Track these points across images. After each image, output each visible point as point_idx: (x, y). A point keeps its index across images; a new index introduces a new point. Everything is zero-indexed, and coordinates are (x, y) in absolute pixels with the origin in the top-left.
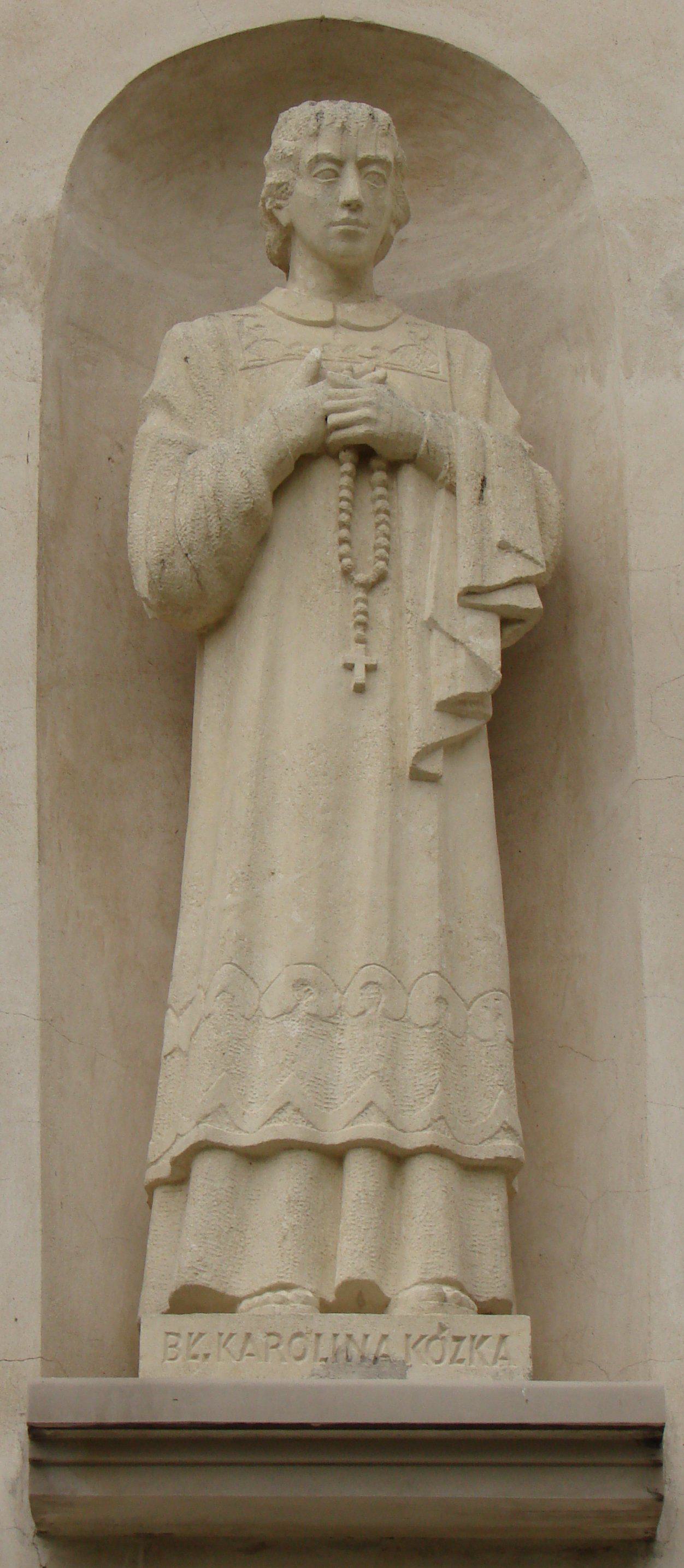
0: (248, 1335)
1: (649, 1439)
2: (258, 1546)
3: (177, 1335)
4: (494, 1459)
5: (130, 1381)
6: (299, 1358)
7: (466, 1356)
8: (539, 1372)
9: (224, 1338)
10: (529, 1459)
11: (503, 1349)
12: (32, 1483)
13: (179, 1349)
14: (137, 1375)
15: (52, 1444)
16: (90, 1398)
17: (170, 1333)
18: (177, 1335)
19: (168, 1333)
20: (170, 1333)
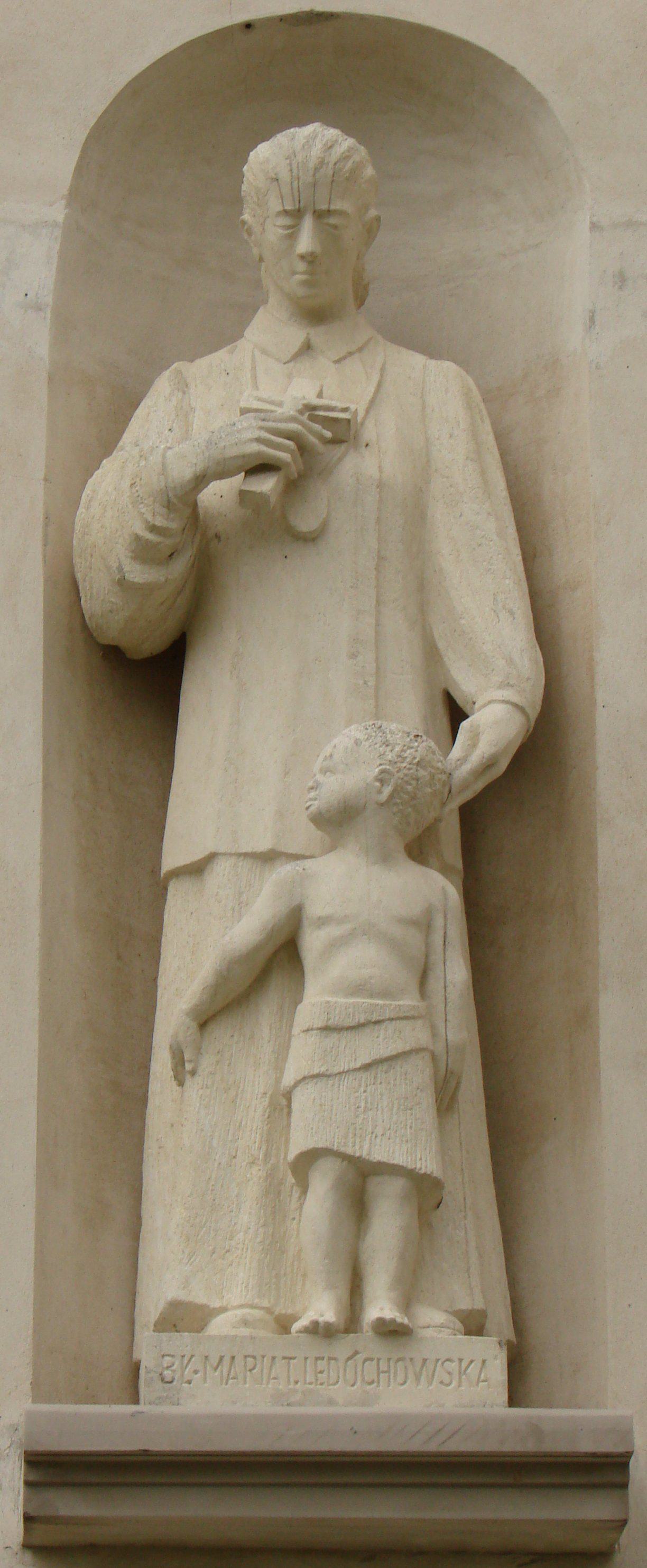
0: (484, 1361)
1: (604, 1470)
2: (461, 1552)
3: (172, 1356)
4: (159, 1479)
5: (132, 1408)
6: (353, 1385)
7: (240, 1376)
8: (513, 1401)
9: (464, 1365)
10: (346, 1479)
11: (483, 1375)
12: (27, 1501)
13: (174, 1371)
14: (136, 1401)
15: (48, 1468)
16: (100, 1425)
17: (249, 1356)
18: (172, 1356)
19: (246, 1357)
20: (249, 1356)
